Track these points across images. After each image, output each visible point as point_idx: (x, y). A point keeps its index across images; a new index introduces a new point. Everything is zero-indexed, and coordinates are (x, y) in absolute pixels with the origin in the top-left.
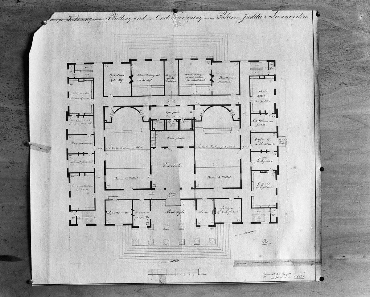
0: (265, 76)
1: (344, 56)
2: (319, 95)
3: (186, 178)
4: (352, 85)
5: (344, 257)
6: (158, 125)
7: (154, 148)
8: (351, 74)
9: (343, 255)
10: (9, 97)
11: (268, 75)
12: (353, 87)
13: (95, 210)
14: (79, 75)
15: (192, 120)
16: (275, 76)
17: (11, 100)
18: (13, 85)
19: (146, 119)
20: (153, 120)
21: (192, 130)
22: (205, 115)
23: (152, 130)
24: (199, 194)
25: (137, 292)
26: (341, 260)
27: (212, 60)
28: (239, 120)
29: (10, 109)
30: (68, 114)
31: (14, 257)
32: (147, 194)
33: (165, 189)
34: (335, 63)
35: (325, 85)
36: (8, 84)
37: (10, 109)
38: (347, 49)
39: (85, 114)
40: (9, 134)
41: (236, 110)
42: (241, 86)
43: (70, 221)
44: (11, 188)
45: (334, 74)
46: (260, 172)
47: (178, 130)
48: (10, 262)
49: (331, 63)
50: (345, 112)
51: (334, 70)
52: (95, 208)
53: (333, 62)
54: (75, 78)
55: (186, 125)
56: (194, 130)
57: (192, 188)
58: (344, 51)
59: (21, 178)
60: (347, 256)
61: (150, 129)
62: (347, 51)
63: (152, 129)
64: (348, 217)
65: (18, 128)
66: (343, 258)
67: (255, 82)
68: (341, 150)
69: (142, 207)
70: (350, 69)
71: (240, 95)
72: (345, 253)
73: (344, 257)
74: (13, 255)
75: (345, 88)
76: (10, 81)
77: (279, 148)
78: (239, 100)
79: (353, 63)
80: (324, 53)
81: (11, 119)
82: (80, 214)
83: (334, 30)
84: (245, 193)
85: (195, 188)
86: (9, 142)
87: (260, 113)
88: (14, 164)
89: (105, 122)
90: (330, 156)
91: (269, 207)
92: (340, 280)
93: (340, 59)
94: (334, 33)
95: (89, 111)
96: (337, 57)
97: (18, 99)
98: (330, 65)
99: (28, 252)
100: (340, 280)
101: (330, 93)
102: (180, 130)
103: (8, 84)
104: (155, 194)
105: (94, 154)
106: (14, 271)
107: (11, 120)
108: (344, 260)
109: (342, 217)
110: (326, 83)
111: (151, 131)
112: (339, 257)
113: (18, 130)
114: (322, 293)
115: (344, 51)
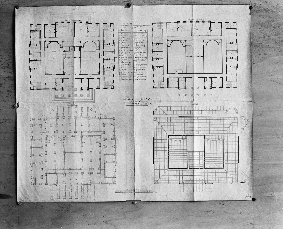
0: (109, 29)
1: (272, 32)
2: (252, 63)
3: (77, 70)
4: (278, 56)
5: (272, 194)
6: (66, 49)
7: (64, 58)
8: (278, 46)
9: (272, 193)
10: (2, 66)
11: (111, 29)
12: (279, 57)
13: (41, 83)
14: (110, 84)
15: (80, 47)
16: (113, 29)
17: (4, 69)
18: (5, 57)
19: (61, 47)
20: (64, 47)
21: (80, 51)
22: (85, 45)
23: (64, 51)
24: (82, 77)
25: (106, 222)
26: (270, 197)
27: (88, 22)
28: (222, 46)
29: (3, 76)
30: (30, 45)
31: (6, 195)
32: (62, 77)
33: (69, 74)
34: (267, 39)
35: (257, 55)
36: (1, 56)
37: (3, 76)
38: (274, 26)
39: (37, 45)
40: (2, 96)
41: (97, 43)
42: (222, 63)
43: (31, 87)
44: (4, 139)
45: (264, 47)
46: (107, 68)
47: (70, 47)
48: (3, 199)
49: (262, 37)
50: (273, 78)
51: (263, 43)
52: (41, 82)
53: (263, 37)
54: (33, 30)
55: (77, 49)
56: (81, 51)
57: (80, 74)
58: (271, 28)
59: (12, 132)
60: (275, 194)
61: (63, 50)
62: (274, 28)
63: (64, 51)
64: (275, 162)
65: (9, 91)
66: (271, 195)
67: (105, 31)
68: (269, 108)
69: (182, 81)
70: (277, 43)
71: (99, 37)
72: (273, 191)
73: (272, 194)
74: (6, 194)
75: (273, 58)
76: (3, 53)
77: (115, 58)
78: (99, 39)
79: (279, 38)
80: (256, 29)
81: (3, 84)
82: (35, 85)
83: (263, 11)
84: (101, 76)
85: (81, 74)
86: (2, 103)
87: (107, 44)
88: (6, 120)
89: (168, 46)
90: (261, 113)
91: (111, 82)
92: (269, 213)
93: (268, 35)
94: (263, 14)
95: (38, 43)
96: (266, 33)
97: (9, 68)
98: (261, 39)
99: (11, 52)
100: (269, 213)
101: (261, 62)
102: (69, 47)
103: (1, 56)
104: (65, 77)
105: (41, 60)
106: (6, 207)
107: (3, 85)
108: (272, 196)
109: (270, 162)
110: (257, 53)
111: (63, 51)
112: (268, 195)
113: (9, 93)
114: (255, 223)
115: (271, 28)
